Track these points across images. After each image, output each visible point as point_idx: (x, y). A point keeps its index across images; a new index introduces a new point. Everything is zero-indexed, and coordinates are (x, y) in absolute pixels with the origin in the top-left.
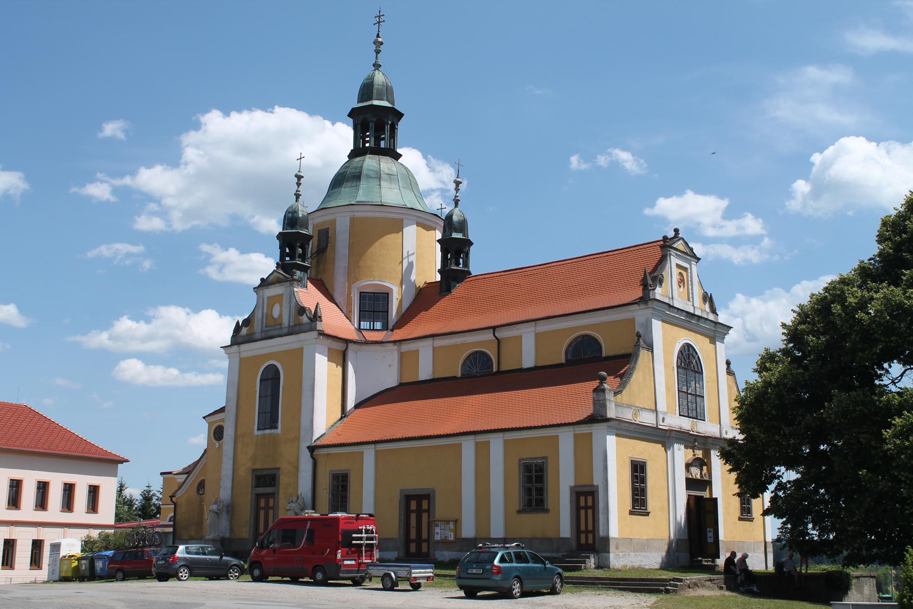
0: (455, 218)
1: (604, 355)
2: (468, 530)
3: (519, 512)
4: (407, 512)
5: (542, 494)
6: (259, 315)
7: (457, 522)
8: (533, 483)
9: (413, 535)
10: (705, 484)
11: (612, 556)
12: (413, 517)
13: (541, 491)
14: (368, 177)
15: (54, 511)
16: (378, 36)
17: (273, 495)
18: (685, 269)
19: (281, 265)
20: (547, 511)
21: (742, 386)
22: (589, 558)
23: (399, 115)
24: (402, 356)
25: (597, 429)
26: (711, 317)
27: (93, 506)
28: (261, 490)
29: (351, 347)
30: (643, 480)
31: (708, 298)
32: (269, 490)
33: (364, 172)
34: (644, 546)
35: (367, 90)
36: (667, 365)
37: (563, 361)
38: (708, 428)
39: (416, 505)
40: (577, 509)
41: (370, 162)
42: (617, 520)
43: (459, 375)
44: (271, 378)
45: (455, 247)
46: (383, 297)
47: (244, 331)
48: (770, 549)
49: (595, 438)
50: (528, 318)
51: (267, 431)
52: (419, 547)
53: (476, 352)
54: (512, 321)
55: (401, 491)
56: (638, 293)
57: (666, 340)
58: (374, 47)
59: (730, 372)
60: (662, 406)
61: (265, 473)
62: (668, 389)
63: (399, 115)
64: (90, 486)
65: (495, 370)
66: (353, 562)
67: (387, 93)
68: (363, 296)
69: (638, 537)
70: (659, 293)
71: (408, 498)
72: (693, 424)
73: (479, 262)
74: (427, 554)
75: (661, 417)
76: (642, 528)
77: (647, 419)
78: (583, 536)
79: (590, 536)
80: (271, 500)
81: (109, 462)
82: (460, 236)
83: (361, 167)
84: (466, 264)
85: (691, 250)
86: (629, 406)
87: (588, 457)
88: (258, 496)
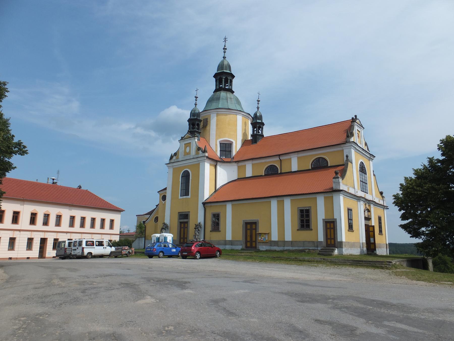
0: (258, 114)
1: (329, 165)
2: (275, 237)
3: (298, 230)
5: (309, 222)
6: (180, 151)
8: (305, 219)
9: (249, 239)
11: (344, 249)
12: (249, 232)
13: (308, 221)
14: (223, 99)
16: (225, 46)
17: (187, 222)
18: (359, 132)
20: (312, 230)
22: (334, 250)
24: (239, 168)
25: (335, 196)
27: (111, 227)
28: (182, 221)
29: (218, 163)
31: (366, 144)
32: (185, 220)
34: (352, 245)
35: (221, 66)
36: (357, 169)
37: (310, 168)
38: (369, 197)
39: (250, 227)
41: (223, 94)
42: (343, 235)
43: (264, 175)
44: (186, 176)
45: (257, 123)
47: (174, 158)
49: (334, 198)
50: (295, 151)
51: (185, 197)
52: (184, 240)
53: (271, 165)
54: (286, 152)
57: (356, 159)
58: (223, 51)
59: (374, 175)
60: (356, 187)
61: (184, 213)
62: (357, 180)
63: (233, 77)
64: (348, 231)
70: (352, 139)
71: (247, 224)
72: (365, 195)
73: (267, 132)
78: (329, 241)
79: (333, 241)
80: (186, 225)
82: (260, 121)
83: (220, 95)
87: (330, 207)
88: (181, 223)
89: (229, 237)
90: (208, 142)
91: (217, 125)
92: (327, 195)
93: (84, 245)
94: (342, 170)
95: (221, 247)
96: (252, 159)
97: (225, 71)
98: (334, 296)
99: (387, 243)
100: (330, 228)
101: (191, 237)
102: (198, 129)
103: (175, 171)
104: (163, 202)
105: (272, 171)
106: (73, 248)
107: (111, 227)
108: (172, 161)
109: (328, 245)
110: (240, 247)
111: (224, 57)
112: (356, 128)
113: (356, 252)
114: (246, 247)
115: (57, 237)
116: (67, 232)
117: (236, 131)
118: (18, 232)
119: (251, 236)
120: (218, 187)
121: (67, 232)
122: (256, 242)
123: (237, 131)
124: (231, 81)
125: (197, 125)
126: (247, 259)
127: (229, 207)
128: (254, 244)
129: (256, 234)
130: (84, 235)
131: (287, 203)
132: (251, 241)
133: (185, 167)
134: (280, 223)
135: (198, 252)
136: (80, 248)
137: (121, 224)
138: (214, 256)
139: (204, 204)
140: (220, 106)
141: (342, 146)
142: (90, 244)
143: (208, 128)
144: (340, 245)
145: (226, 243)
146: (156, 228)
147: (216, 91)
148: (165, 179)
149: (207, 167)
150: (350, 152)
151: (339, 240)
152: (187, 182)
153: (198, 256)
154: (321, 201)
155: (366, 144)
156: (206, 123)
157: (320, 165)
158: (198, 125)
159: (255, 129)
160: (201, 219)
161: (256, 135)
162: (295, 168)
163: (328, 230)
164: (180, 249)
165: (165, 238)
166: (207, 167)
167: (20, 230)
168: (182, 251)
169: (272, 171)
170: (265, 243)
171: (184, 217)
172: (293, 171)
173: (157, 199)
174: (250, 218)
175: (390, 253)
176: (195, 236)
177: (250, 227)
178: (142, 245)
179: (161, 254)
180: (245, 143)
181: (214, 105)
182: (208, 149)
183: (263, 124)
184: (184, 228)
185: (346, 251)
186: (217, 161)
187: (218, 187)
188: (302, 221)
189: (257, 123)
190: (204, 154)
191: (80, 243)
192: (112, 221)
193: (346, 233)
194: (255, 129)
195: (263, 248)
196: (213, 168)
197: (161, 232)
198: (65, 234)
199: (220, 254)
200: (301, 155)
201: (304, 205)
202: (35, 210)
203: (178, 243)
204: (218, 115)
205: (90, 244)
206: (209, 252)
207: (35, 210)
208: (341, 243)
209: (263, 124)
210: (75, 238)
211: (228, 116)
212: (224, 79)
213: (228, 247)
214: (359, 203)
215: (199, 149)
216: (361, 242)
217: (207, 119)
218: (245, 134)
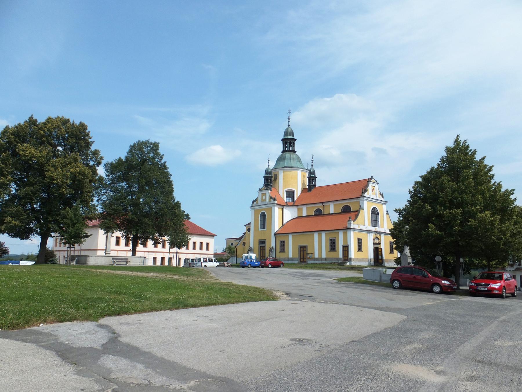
2: (316, 256)
7: (313, 254)
9: (302, 257)
10: (379, 244)
11: (352, 262)
12: (302, 252)
15: (198, 250)
19: (265, 185)
25: (348, 231)
26: (382, 199)
27: (207, 249)
31: (381, 194)
32: (264, 245)
35: (286, 133)
36: (368, 213)
39: (303, 249)
41: (288, 155)
44: (263, 215)
45: (312, 179)
46: (293, 192)
47: (255, 203)
52: (304, 260)
57: (367, 207)
59: (387, 214)
62: (368, 219)
66: (461, 288)
70: (366, 195)
76: (360, 255)
84: (315, 184)
87: (346, 238)
89: (290, 256)
90: (278, 191)
91: (283, 179)
93: (202, 261)
94: (357, 213)
95: (283, 262)
97: (289, 137)
98: (481, 331)
101: (267, 256)
102: (271, 183)
103: (256, 212)
106: (195, 263)
107: (207, 249)
108: (254, 205)
110: (297, 262)
111: (289, 126)
112: (371, 185)
114: (301, 261)
118: (147, 253)
119: (303, 255)
120: (284, 223)
124: (294, 144)
125: (270, 180)
126: (301, 268)
127: (290, 237)
130: (119, 252)
131: (323, 235)
133: (264, 209)
135: (270, 264)
136: (200, 263)
137: (217, 245)
138: (280, 267)
139: (275, 234)
140: (286, 165)
142: (205, 260)
143: (277, 181)
144: (350, 260)
145: (289, 259)
146: (244, 249)
147: (282, 152)
148: (249, 216)
149: (277, 210)
150: (363, 203)
152: (263, 220)
153: (270, 266)
156: (276, 177)
157: (346, 210)
158: (270, 180)
160: (273, 245)
162: (332, 211)
164: (260, 263)
165: (251, 257)
166: (277, 210)
167: (148, 252)
168: (261, 264)
169: (319, 213)
171: (262, 243)
172: (331, 213)
173: (244, 230)
174: (303, 244)
177: (303, 249)
178: (235, 261)
179: (249, 266)
180: (304, 190)
181: (281, 164)
182: (277, 198)
184: (263, 250)
185: (353, 263)
186: (283, 206)
187: (284, 223)
189: (312, 179)
190: (274, 202)
191: (200, 260)
192: (208, 244)
193: (355, 253)
195: (310, 262)
197: (248, 253)
199: (283, 265)
200: (335, 203)
201: (332, 236)
203: (259, 260)
204: (284, 172)
205: (205, 260)
206: (277, 264)
208: (351, 258)
210: (197, 257)
212: (289, 143)
213: (290, 262)
215: (271, 198)
216: (369, 258)
217: (276, 174)
218: (303, 184)
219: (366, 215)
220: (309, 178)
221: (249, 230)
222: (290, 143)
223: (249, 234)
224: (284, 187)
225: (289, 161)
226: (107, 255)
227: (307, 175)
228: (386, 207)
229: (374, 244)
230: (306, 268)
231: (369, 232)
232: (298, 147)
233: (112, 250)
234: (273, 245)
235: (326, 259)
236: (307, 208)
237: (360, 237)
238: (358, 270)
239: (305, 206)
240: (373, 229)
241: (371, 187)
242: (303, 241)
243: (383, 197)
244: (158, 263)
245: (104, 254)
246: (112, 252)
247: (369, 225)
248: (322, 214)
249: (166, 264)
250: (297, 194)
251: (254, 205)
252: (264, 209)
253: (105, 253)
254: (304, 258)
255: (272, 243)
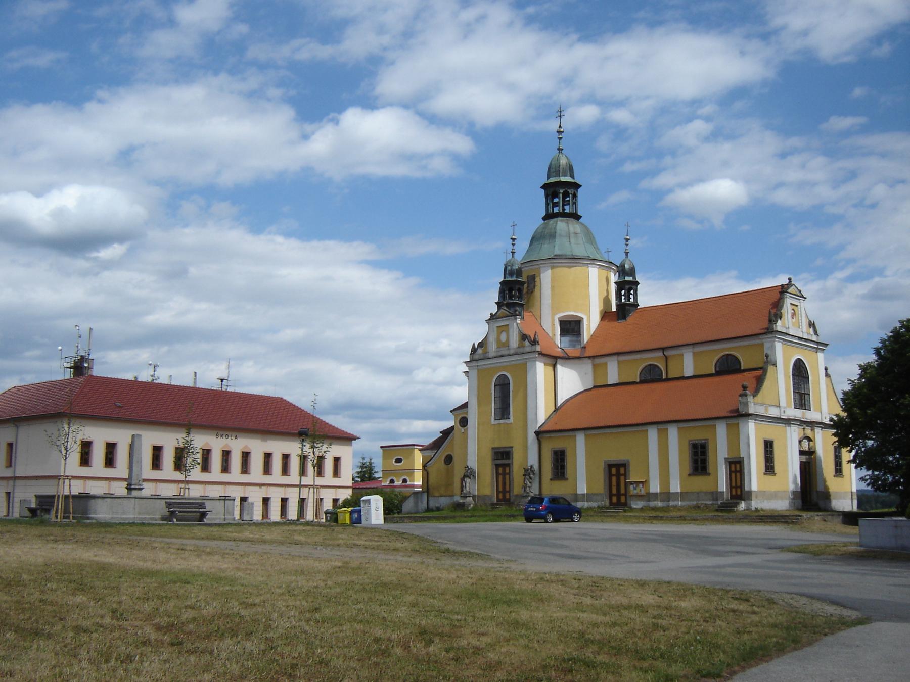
0: (627, 266)
2: (655, 487)
3: (689, 475)
4: (610, 475)
6: (492, 339)
8: (699, 458)
9: (614, 491)
12: (614, 479)
14: (561, 236)
15: (235, 474)
16: (560, 127)
17: (508, 465)
20: (709, 474)
21: (841, 396)
22: (738, 503)
23: (577, 186)
24: (595, 366)
25: (741, 422)
26: (814, 338)
30: (772, 453)
31: (812, 325)
32: (506, 462)
33: (558, 232)
34: (774, 495)
35: (553, 170)
36: (786, 375)
37: (714, 372)
38: (812, 415)
39: (616, 472)
40: (730, 472)
41: (561, 225)
42: (755, 479)
44: (503, 386)
45: (627, 286)
47: (480, 351)
48: (855, 497)
49: (740, 425)
51: (502, 421)
52: (504, 496)
53: (650, 365)
55: (605, 462)
56: (766, 324)
57: (783, 357)
59: (827, 375)
60: (783, 403)
62: (787, 390)
63: (577, 186)
64: (765, 474)
65: (664, 377)
67: (570, 170)
68: (561, 322)
69: (773, 489)
70: (779, 326)
71: (610, 466)
72: (803, 413)
74: (625, 504)
75: (782, 410)
76: (771, 484)
77: (773, 412)
78: (734, 490)
79: (739, 490)
81: (347, 438)
82: (630, 279)
83: (555, 228)
85: (800, 291)
86: (762, 404)
87: (735, 439)
90: (538, 319)
91: (553, 288)
92: (731, 421)
94: (759, 374)
96: (618, 354)
97: (563, 179)
99: (854, 490)
100: (736, 472)
101: (517, 489)
104: (463, 430)
105: (651, 376)
109: (732, 497)
112: (788, 301)
113: (782, 505)
114: (611, 503)
115: (85, 488)
116: (261, 485)
117: (588, 295)
119: (504, 484)
120: (559, 403)
121: (261, 485)
122: (625, 495)
123: (588, 293)
124: (575, 196)
127: (580, 439)
128: (623, 499)
129: (626, 483)
132: (619, 495)
133: (504, 368)
134: (661, 465)
139: (538, 434)
140: (557, 252)
141: (761, 337)
147: (544, 219)
149: (541, 369)
150: (773, 348)
151: (747, 489)
154: (721, 430)
155: (812, 325)
157: (728, 366)
158: (520, 291)
159: (623, 292)
160: (533, 460)
161: (625, 304)
162: (689, 371)
163: (733, 475)
169: (651, 376)
170: (640, 497)
171: (502, 457)
174: (615, 457)
175: (859, 506)
176: (525, 487)
177: (616, 472)
180: (606, 315)
181: (546, 250)
182: (540, 338)
183: (637, 283)
184: (504, 474)
185: (755, 504)
187: (559, 403)
188: (695, 462)
189: (627, 286)
193: (759, 478)
194: (623, 292)
196: (551, 369)
198: (257, 488)
201: (698, 435)
202: (207, 443)
206: (563, 510)
207: (207, 443)
208: (750, 492)
209: (637, 283)
211: (573, 269)
214: (788, 428)
215: (524, 337)
218: (607, 301)
219: (780, 380)
220: (620, 286)
221: (464, 422)
222: (566, 195)
223: (465, 434)
224: (555, 310)
225: (567, 240)
226: (135, 493)
227: (614, 278)
228: (825, 358)
229: (802, 453)
230: (627, 520)
231: (788, 422)
232: (584, 202)
233: (145, 480)
234: (533, 460)
235: (683, 495)
236: (694, 353)
237: (769, 438)
238: (786, 522)
239: (615, 357)
240: (798, 414)
241: (790, 307)
242: (616, 449)
243: (816, 333)
244: (275, 515)
245: (124, 492)
246: (145, 485)
247: (788, 405)
248: (660, 380)
249: (293, 514)
250: (591, 323)
251: (476, 357)
252: (504, 368)
253: (129, 488)
254: (618, 490)
255: (528, 455)
